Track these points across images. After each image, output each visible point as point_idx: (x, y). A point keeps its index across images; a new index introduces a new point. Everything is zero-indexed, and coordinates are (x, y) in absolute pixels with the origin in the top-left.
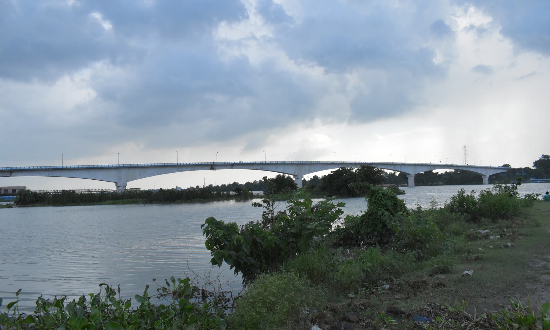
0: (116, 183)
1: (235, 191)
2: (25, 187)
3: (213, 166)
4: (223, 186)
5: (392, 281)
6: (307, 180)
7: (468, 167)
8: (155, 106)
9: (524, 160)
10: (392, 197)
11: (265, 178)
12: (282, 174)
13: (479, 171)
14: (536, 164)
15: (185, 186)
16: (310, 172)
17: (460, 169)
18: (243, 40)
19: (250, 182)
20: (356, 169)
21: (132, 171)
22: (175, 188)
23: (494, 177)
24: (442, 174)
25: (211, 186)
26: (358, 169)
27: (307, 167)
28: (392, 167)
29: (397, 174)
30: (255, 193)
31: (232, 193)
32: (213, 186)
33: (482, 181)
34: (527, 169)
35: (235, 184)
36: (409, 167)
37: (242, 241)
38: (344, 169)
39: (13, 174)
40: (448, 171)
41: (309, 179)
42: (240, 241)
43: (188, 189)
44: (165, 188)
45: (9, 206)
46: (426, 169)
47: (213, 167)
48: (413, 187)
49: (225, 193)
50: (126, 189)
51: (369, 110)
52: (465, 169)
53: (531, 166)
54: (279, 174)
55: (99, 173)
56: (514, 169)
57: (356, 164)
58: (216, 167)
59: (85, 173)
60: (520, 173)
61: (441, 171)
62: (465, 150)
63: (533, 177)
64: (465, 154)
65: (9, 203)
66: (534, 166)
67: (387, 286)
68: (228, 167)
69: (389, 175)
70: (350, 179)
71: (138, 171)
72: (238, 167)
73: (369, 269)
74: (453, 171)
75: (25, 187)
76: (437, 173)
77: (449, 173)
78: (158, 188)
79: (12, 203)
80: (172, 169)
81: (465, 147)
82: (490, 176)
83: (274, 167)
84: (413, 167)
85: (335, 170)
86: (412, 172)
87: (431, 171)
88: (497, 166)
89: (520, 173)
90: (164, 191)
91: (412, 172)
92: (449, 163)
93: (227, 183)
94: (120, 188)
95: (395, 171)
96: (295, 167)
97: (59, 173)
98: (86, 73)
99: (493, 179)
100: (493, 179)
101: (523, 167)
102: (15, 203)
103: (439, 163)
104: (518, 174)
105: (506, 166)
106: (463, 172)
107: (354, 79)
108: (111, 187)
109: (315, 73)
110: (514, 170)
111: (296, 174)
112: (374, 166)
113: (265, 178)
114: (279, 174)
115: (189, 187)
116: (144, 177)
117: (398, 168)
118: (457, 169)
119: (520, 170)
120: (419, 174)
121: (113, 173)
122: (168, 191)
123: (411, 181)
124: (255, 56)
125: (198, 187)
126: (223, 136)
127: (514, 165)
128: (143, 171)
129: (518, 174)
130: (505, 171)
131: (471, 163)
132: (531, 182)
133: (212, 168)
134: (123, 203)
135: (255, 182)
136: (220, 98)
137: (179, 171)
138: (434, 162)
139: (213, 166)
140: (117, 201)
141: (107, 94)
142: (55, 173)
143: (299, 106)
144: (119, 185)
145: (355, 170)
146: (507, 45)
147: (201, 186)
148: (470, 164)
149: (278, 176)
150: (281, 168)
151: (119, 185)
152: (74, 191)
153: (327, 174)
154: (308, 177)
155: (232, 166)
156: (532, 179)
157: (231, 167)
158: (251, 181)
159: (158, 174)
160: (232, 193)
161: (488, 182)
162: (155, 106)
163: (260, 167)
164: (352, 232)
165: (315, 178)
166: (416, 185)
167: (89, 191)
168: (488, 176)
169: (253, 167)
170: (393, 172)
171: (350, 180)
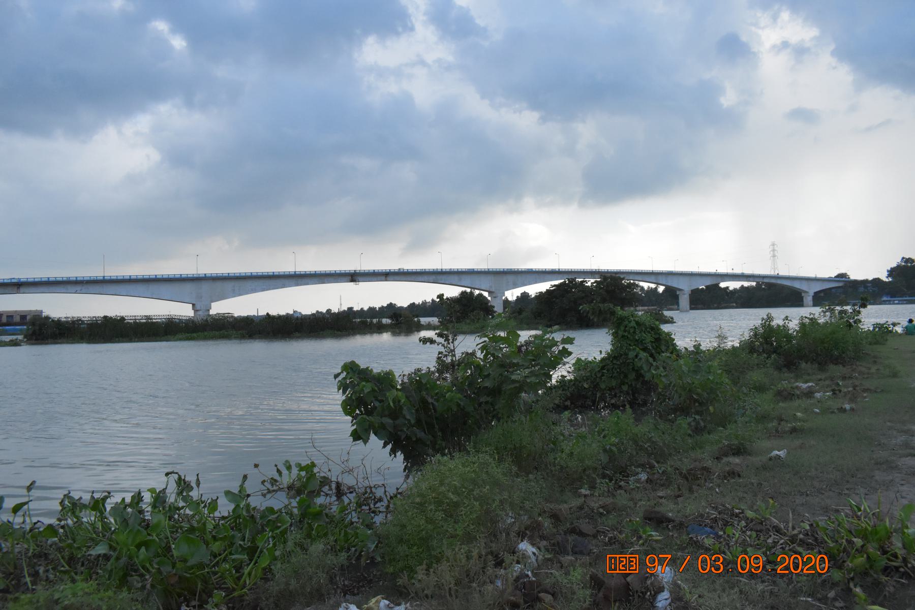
0: (193, 305)
1: (390, 317)
2: (41, 312)
3: (353, 277)
4: (372, 310)
5: (652, 467)
6: (510, 299)
7: (778, 277)
8: (257, 177)
9: (872, 267)
10: (652, 329)
11: (441, 296)
12: (468, 290)
13: (797, 285)
14: (892, 272)
15: (307, 309)
16: (515, 286)
17: (766, 280)
18: (404, 67)
19: (417, 303)
20: (593, 280)
21: (219, 284)
22: (291, 312)
23: (822, 295)
24: (735, 289)
25: (350, 309)
26: (596, 282)
27: (511, 278)
28: (653, 278)
29: (661, 289)
30: (424, 320)
31: (386, 321)
32: (355, 309)
33: (802, 301)
34: (877, 281)
35: (391, 306)
36: (681, 278)
37: (403, 401)
38: (572, 281)
39: (22, 289)
40: (746, 284)
41: (515, 298)
42: (399, 401)
43: (313, 314)
44: (274, 312)
45: (15, 343)
46: (709, 282)
47: (355, 278)
48: (687, 311)
49: (375, 321)
50: (209, 315)
51: (613, 183)
52: (773, 281)
53: (884, 277)
54: (464, 289)
55: (164, 288)
56: (856, 281)
57: (592, 273)
58: (359, 278)
59: (141, 288)
60: (866, 287)
61: (733, 285)
62: (774, 250)
63: (887, 294)
64: (774, 256)
65: (14, 337)
66: (889, 276)
67: (643, 477)
68: (379, 278)
69: (647, 291)
70: (583, 298)
71: (229, 285)
72: (396, 277)
73: (614, 448)
74: (754, 284)
75: (41, 312)
76: (727, 288)
77: (747, 288)
78: (262, 313)
79: (20, 337)
80: (286, 281)
81: (773, 245)
82: (815, 293)
83: (455, 279)
84: (687, 279)
85: (557, 282)
86: (686, 287)
87: (717, 285)
88: (826, 276)
89: (866, 287)
90: (274, 317)
91: (686, 287)
92: (748, 271)
93: (377, 305)
94: (200, 313)
95: (658, 284)
96: (490, 278)
97: (98, 288)
98: (142, 122)
99: (820, 298)
100: (820, 298)
101: (870, 278)
102: (25, 337)
103: (730, 271)
104: (862, 289)
105: (842, 276)
106: (770, 286)
107: (590, 131)
108: (184, 311)
109: (524, 121)
110: (856, 282)
111: (493, 290)
112: (622, 276)
113: (441, 296)
114: (464, 289)
115: (314, 312)
116: (240, 295)
117: (662, 280)
118: (761, 280)
119: (865, 282)
120: (698, 289)
121: (188, 287)
122: (279, 317)
123: (684, 301)
124: (423, 92)
125: (329, 311)
126: (370, 226)
127: (855, 275)
128: (237, 284)
129: (862, 289)
130: (841, 284)
131: (784, 271)
132: (884, 303)
133: (352, 281)
134: (205, 338)
135: (424, 303)
136: (365, 163)
137: (297, 285)
138: (722, 270)
139: (353, 277)
140: (195, 335)
141: (178, 157)
142: (91, 288)
143: (497, 177)
144: (198, 307)
145: (590, 282)
146: (844, 75)
147: (335, 310)
148: (783, 272)
149: (463, 293)
150: (467, 280)
151: (198, 307)
152: (123, 319)
153: (544, 290)
154: (512, 295)
155: (386, 275)
156: (885, 298)
157: (383, 278)
158: (418, 301)
159: (263, 290)
160: (386, 321)
161: (811, 303)
162: (257, 177)
163: (432, 278)
164: (586, 386)
165: (525, 295)
166: (691, 309)
167: (148, 318)
168: (811, 293)
169: (420, 278)
170: (653, 286)
171: (581, 300)
